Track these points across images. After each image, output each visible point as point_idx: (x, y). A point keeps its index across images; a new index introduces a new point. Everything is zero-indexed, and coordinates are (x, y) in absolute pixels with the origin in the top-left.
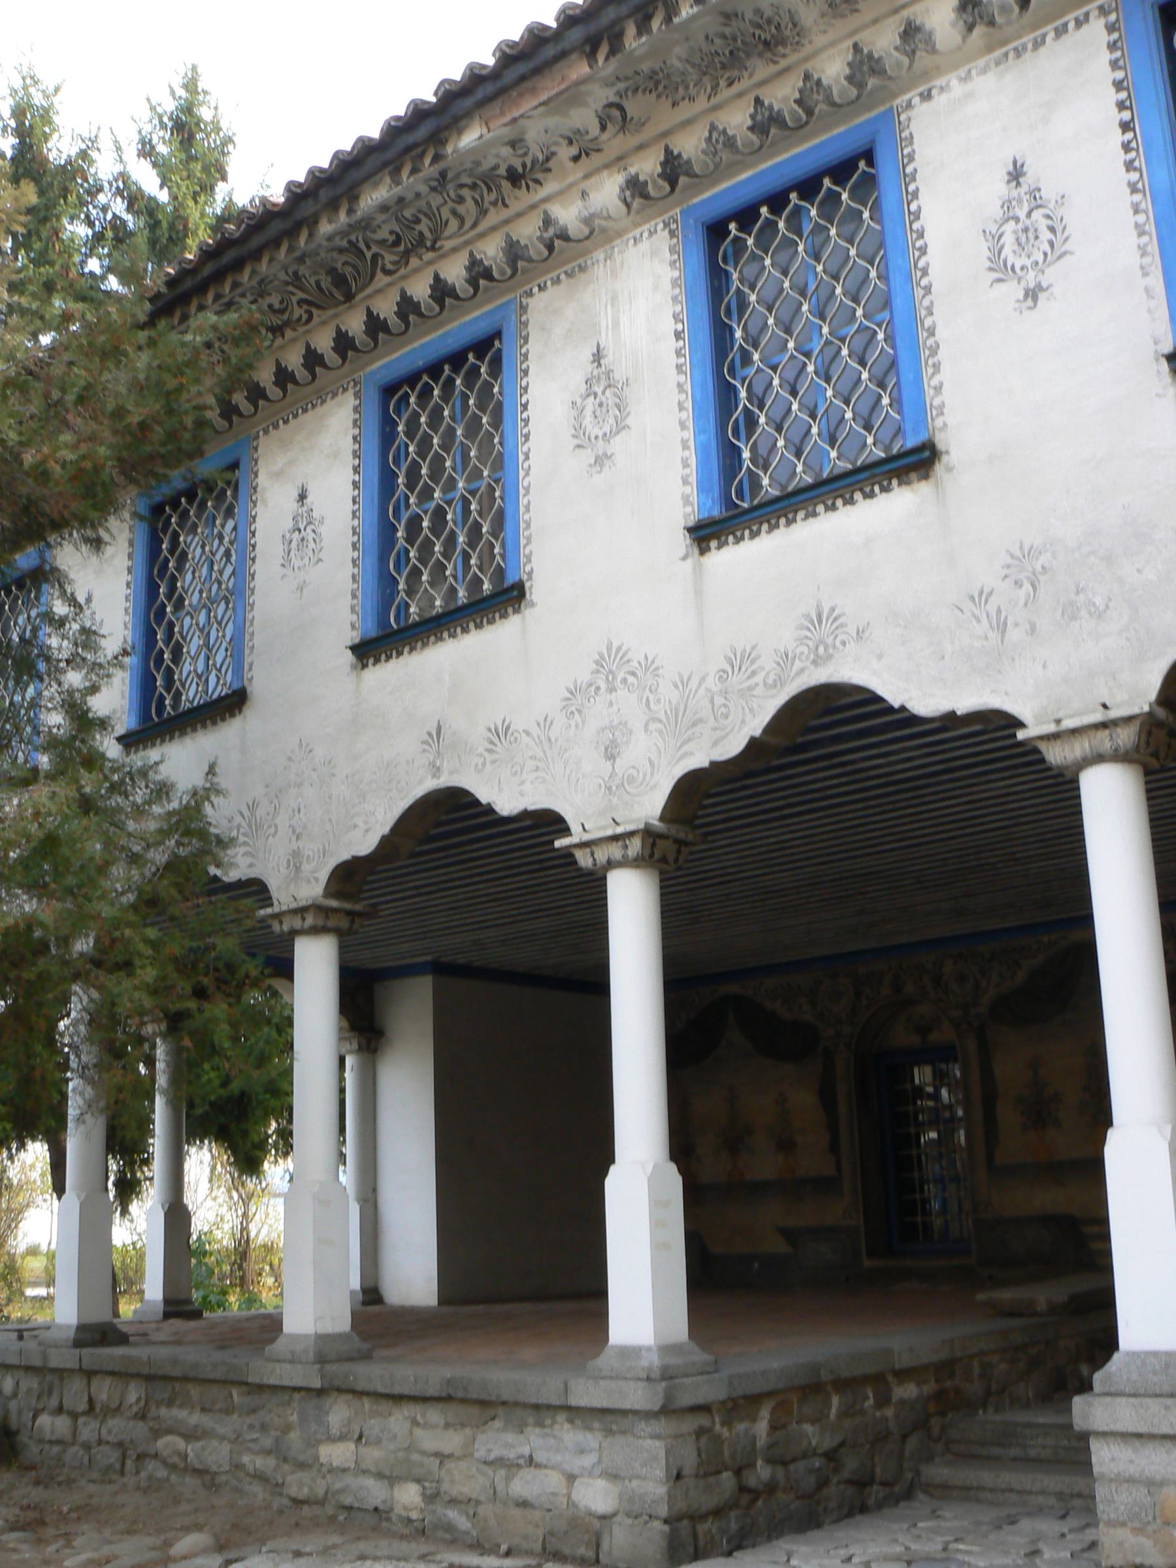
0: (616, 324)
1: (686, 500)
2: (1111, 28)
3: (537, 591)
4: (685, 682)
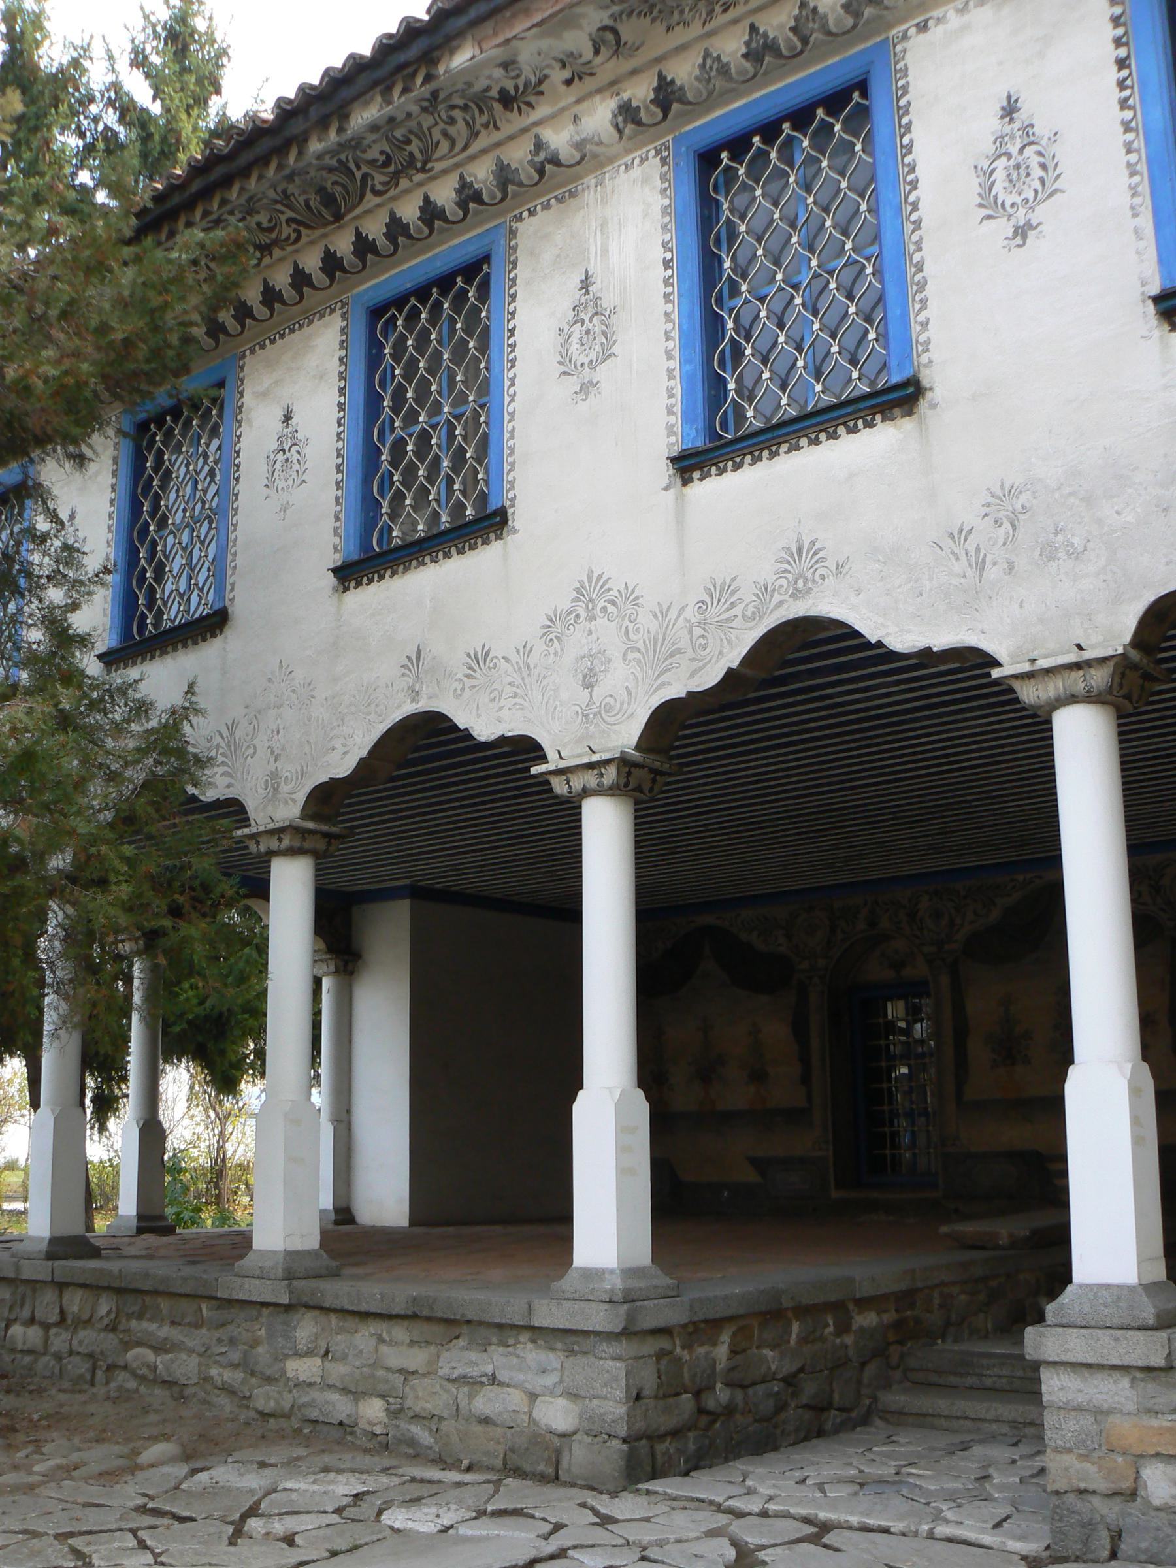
0: (605, 251)
3: (519, 518)
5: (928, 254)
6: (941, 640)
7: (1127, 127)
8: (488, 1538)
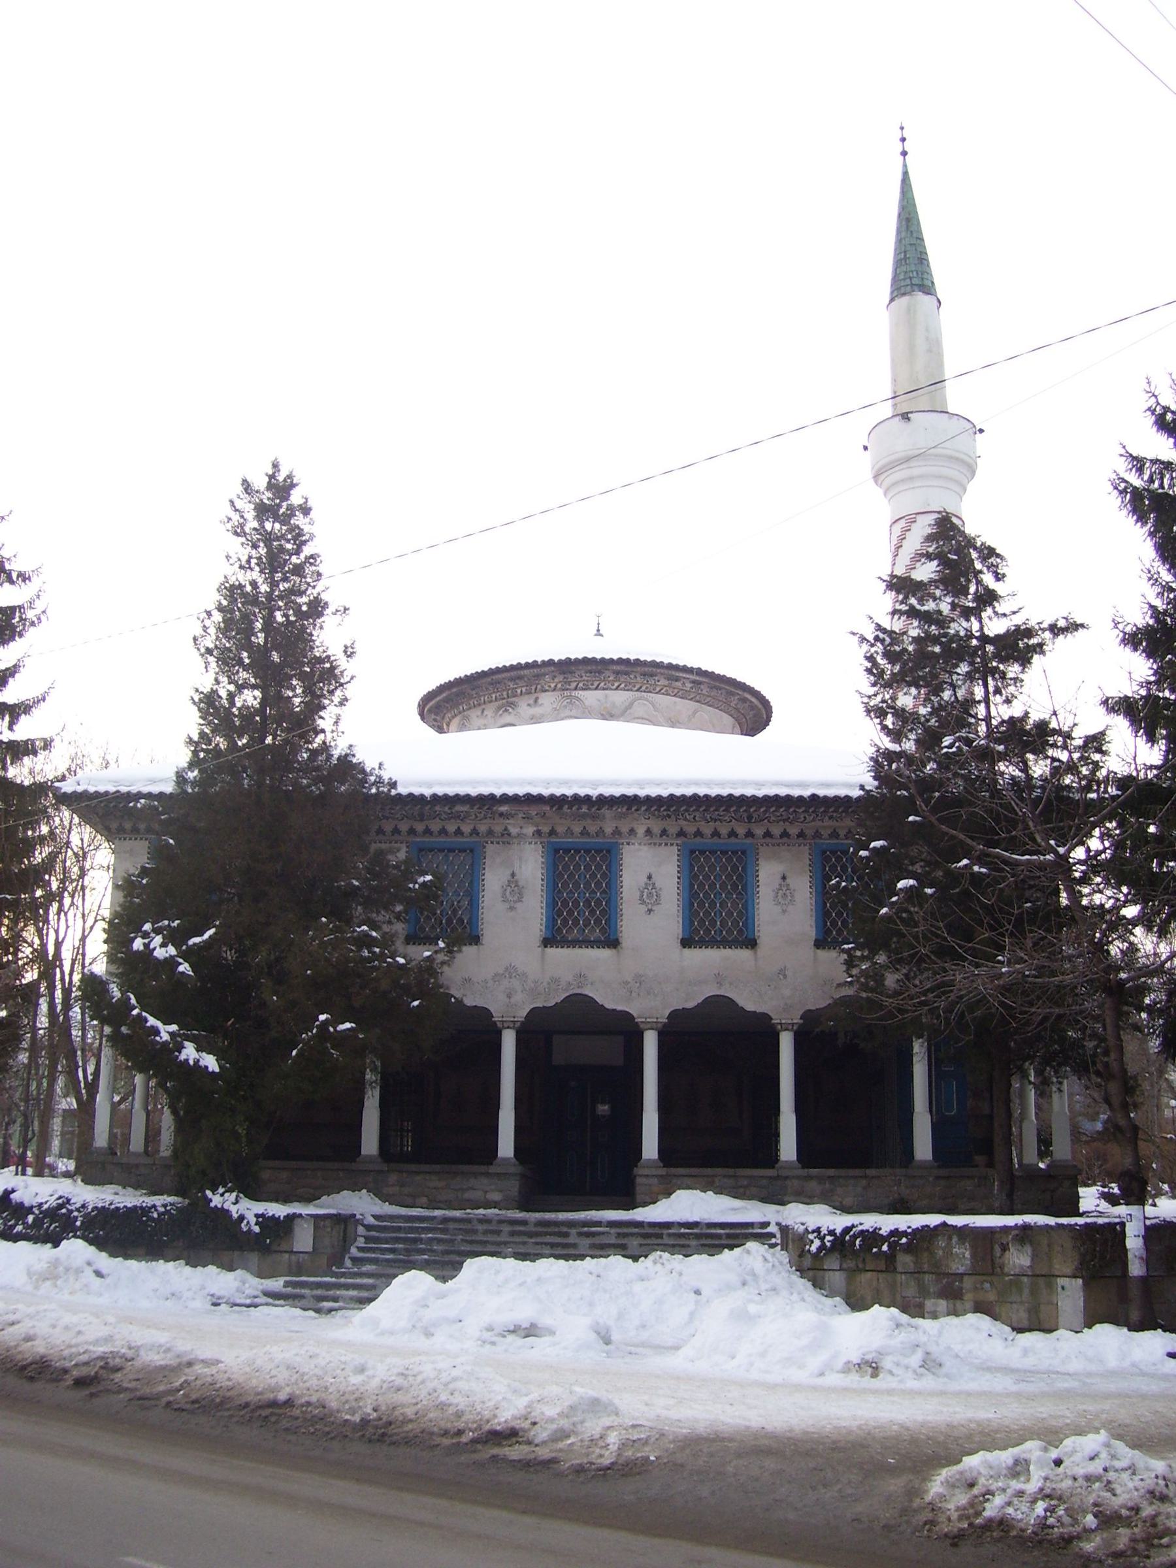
0: (520, 867)
1: (541, 931)
2: (679, 850)
3: (485, 940)
4: (537, 982)
5: (624, 906)
6: (619, 1008)
7: (678, 894)
8: (603, 1233)
